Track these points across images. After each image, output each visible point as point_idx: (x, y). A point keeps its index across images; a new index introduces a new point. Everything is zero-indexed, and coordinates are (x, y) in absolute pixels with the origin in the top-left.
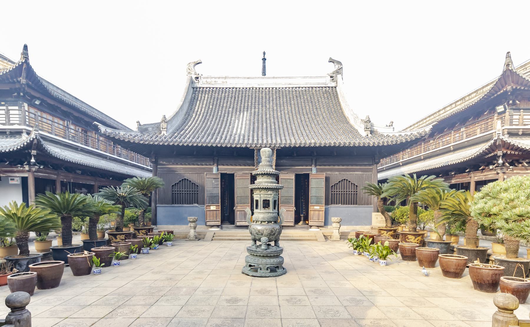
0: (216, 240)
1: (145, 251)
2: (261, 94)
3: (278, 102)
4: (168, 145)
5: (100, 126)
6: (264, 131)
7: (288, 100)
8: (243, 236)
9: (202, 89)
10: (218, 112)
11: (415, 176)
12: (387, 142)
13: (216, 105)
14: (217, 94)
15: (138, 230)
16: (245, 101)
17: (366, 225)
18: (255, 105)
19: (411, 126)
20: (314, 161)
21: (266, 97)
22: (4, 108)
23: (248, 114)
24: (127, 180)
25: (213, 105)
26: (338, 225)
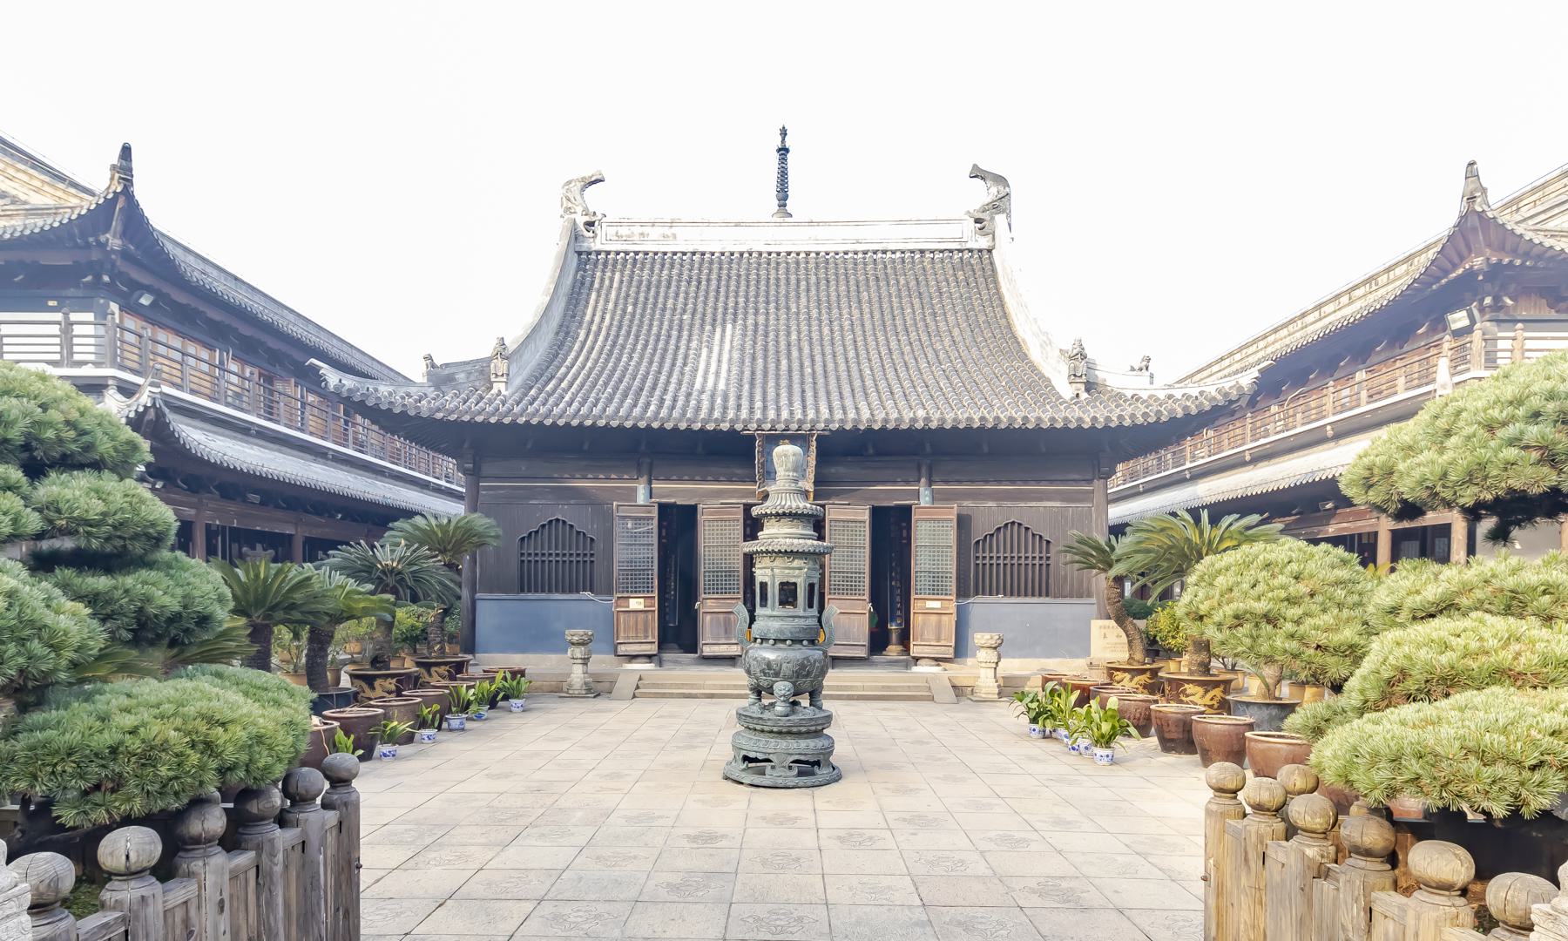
0: (645, 695)
1: (455, 723)
2: (773, 272)
4: (514, 424)
5: (325, 369)
6: (784, 383)
7: (853, 288)
8: (722, 687)
9: (603, 256)
10: (651, 325)
11: (1205, 515)
12: (1133, 416)
13: (645, 304)
14: (646, 272)
15: (427, 666)
16: (727, 292)
17: (1077, 657)
18: (756, 303)
19: (1222, 359)
20: (924, 470)
21: (788, 280)
22: (58, 316)
23: (738, 332)
24: (396, 524)
25: (635, 305)
26: (993, 656)
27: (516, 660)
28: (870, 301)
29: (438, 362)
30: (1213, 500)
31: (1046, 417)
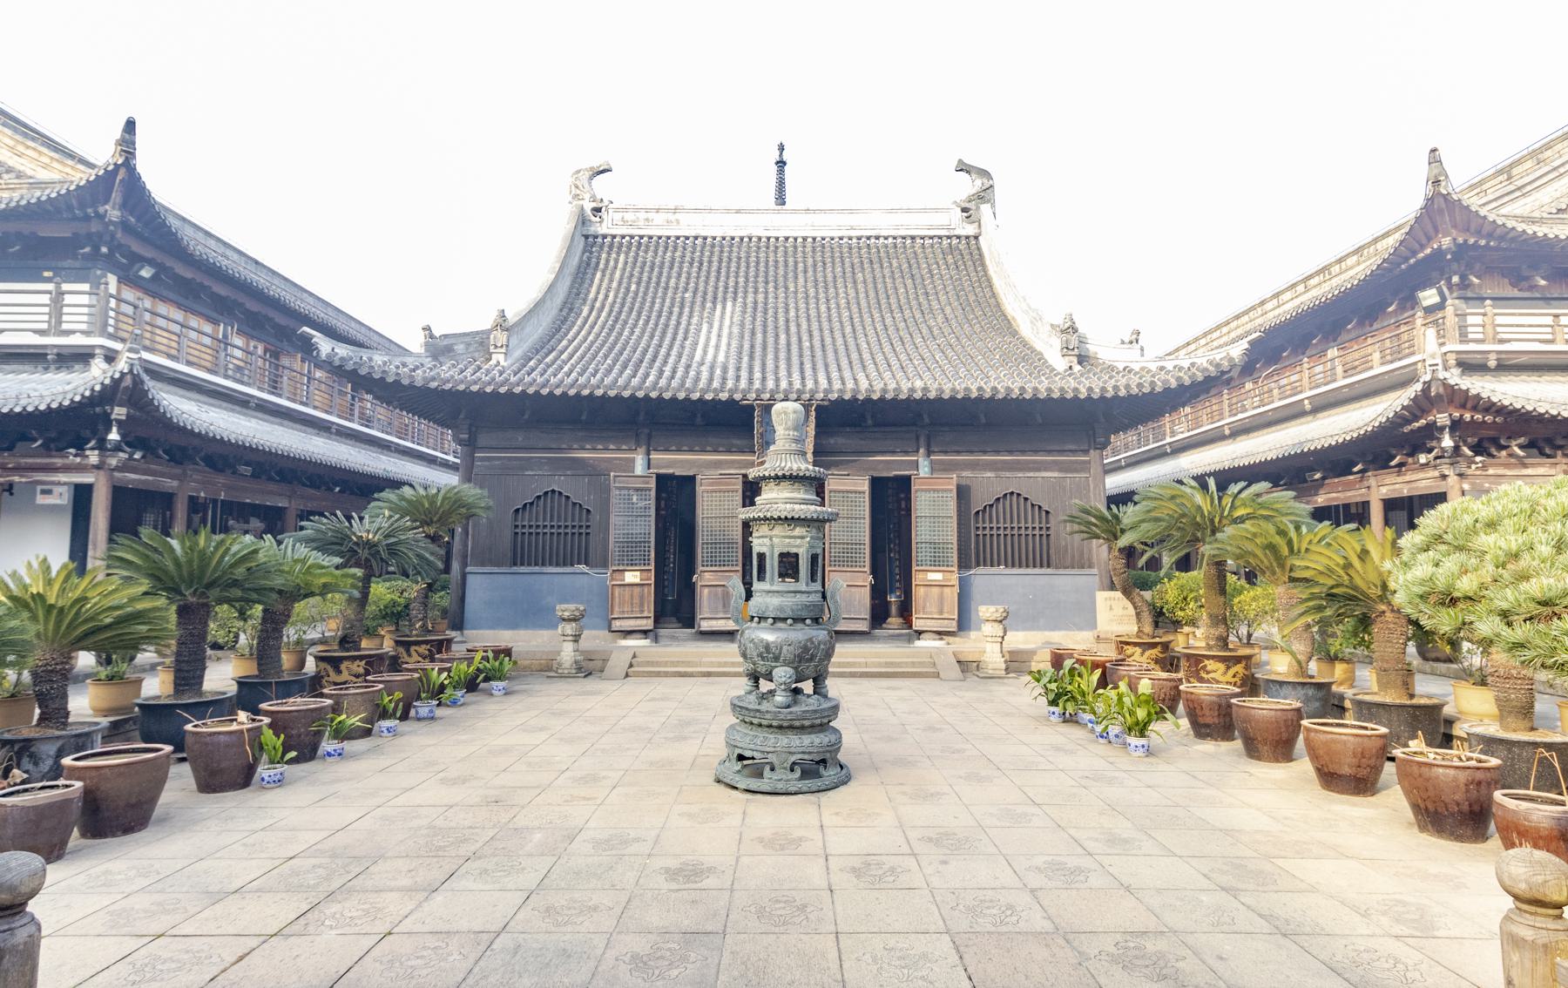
0: (638, 674)
2: (771, 255)
3: (820, 275)
4: (510, 394)
6: (782, 355)
7: (848, 270)
8: (720, 664)
10: (653, 303)
11: (1212, 482)
12: (1127, 386)
13: (648, 282)
14: (650, 253)
15: (407, 645)
17: (1081, 629)
19: (1188, 344)
20: (922, 440)
21: (786, 262)
22: (50, 287)
24: (383, 495)
25: (638, 284)
26: (997, 630)
27: (504, 637)
28: (865, 282)
29: (437, 333)
30: (1218, 467)
31: (1042, 388)
